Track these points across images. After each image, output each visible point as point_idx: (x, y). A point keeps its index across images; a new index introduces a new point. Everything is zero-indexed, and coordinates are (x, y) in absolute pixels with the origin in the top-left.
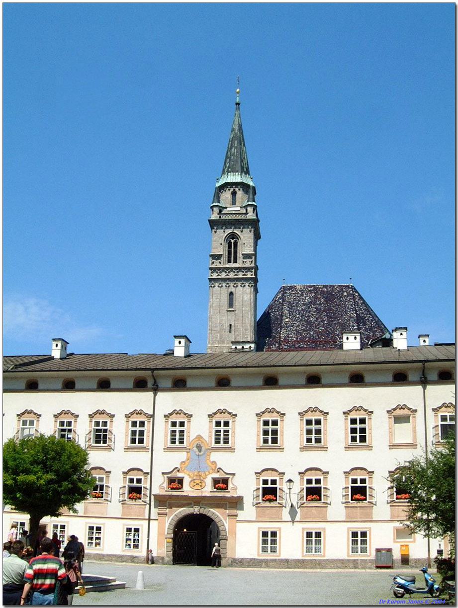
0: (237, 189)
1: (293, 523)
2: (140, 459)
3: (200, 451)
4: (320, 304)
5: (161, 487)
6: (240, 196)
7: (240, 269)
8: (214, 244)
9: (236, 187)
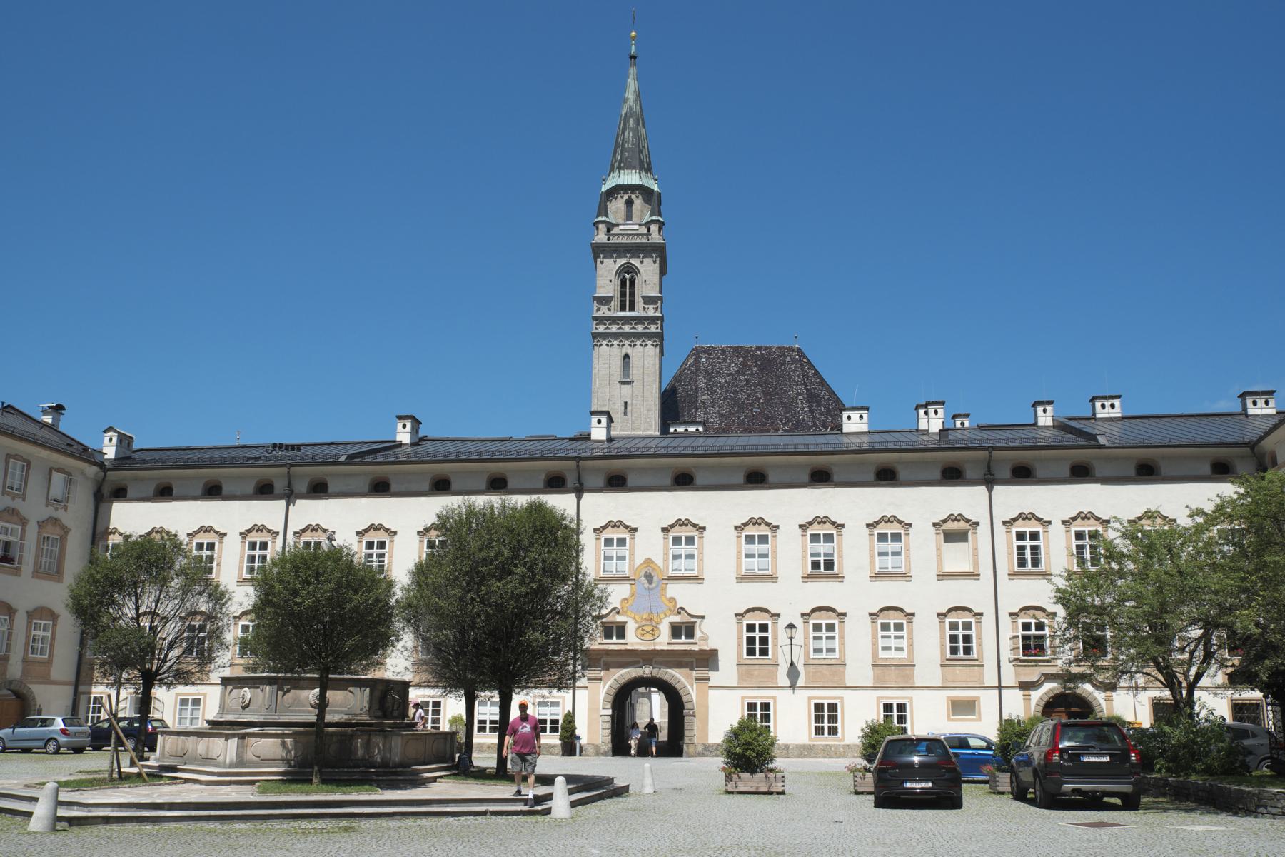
0: (633, 197)
3: (650, 582)
4: (752, 374)
7: (639, 320)
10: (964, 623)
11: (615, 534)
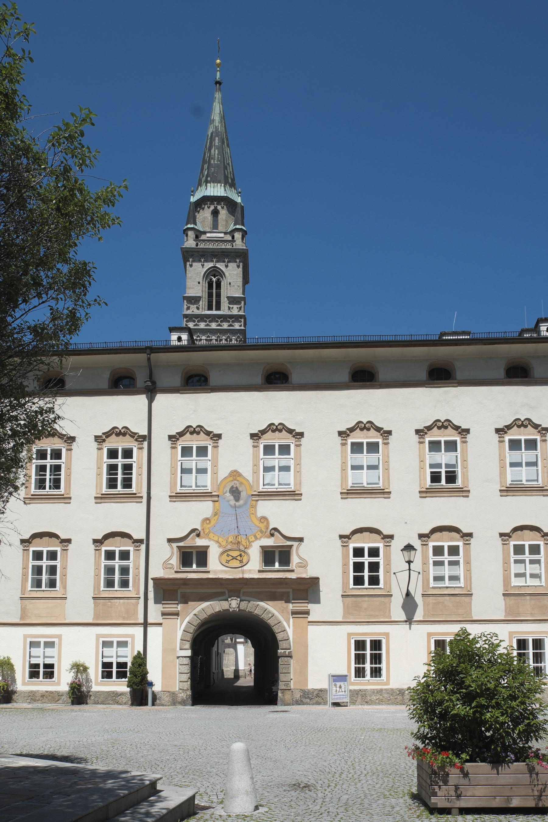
0: (219, 207)
1: (410, 624)
2: (126, 517)
3: (237, 499)
5: (166, 565)
6: (224, 217)
7: (225, 318)
9: (217, 204)
11: (194, 442)
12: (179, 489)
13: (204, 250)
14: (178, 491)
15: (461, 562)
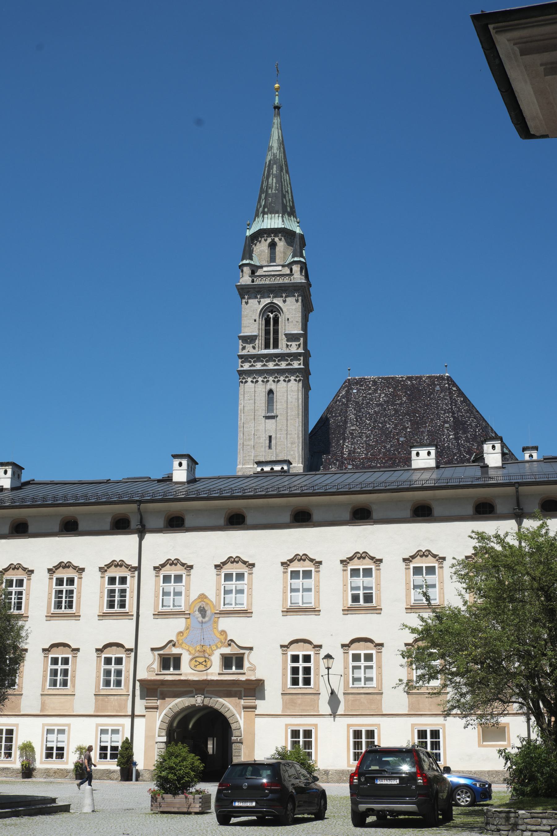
0: (276, 239)
1: (334, 717)
2: (121, 631)
3: (204, 616)
4: (401, 404)
6: (282, 249)
7: (282, 357)
8: (246, 321)
10: (365, 655)
11: (172, 571)
12: (160, 609)
13: (261, 286)
14: (160, 610)
15: (374, 666)
